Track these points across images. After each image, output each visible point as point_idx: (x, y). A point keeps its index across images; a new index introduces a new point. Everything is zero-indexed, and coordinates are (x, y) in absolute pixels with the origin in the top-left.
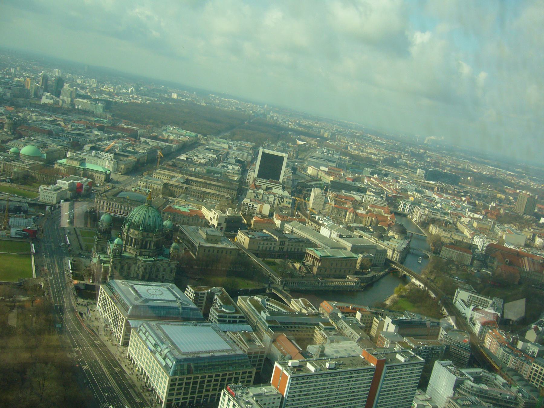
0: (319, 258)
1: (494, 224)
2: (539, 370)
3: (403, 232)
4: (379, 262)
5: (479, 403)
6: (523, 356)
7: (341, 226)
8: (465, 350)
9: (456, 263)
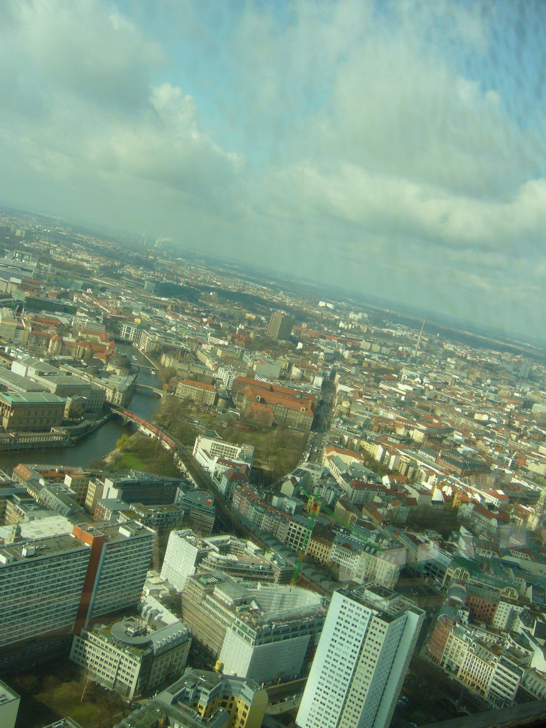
1: (243, 351)
2: (297, 530)
5: (227, 578)
7: (41, 360)
9: (196, 403)
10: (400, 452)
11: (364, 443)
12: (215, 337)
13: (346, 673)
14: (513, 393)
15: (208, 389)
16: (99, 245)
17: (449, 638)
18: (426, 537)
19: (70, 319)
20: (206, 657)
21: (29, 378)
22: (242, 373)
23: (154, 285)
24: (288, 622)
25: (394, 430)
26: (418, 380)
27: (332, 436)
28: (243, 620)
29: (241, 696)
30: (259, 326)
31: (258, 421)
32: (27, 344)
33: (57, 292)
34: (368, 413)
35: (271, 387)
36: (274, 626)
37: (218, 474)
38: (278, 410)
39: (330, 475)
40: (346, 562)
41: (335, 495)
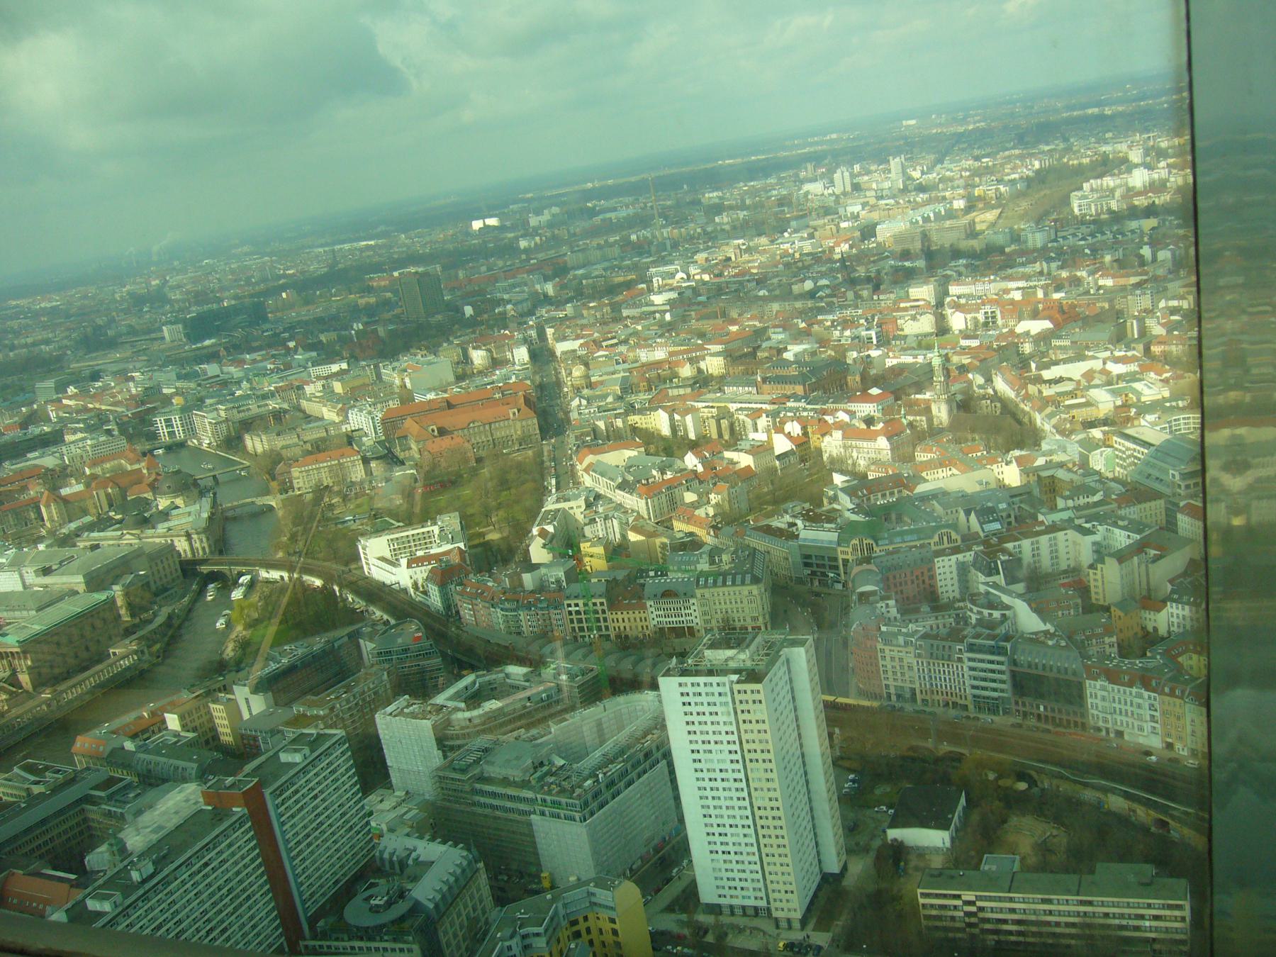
0: (18, 650)
1: (376, 366)
2: (581, 608)
3: (187, 486)
4: (170, 578)
5: (496, 743)
6: (541, 601)
7: (41, 547)
8: (427, 655)
9: (336, 488)
10: (696, 404)
11: (634, 419)
12: (319, 365)
13: (737, 790)
14: (838, 226)
15: (343, 456)
16: (54, 304)
17: (879, 655)
18: (788, 518)
19: (57, 455)
20: (522, 877)
21: (32, 586)
22: (391, 402)
23: (180, 326)
24: (621, 759)
25: (676, 376)
26: (680, 275)
27: (578, 432)
28: (549, 793)
29: (597, 909)
30: (389, 311)
31: (449, 466)
32: (5, 533)
33: (16, 419)
34: (620, 367)
35: (448, 402)
36: (600, 776)
37: (420, 585)
38: (480, 432)
39: (598, 497)
40: (681, 619)
41: (621, 524)
